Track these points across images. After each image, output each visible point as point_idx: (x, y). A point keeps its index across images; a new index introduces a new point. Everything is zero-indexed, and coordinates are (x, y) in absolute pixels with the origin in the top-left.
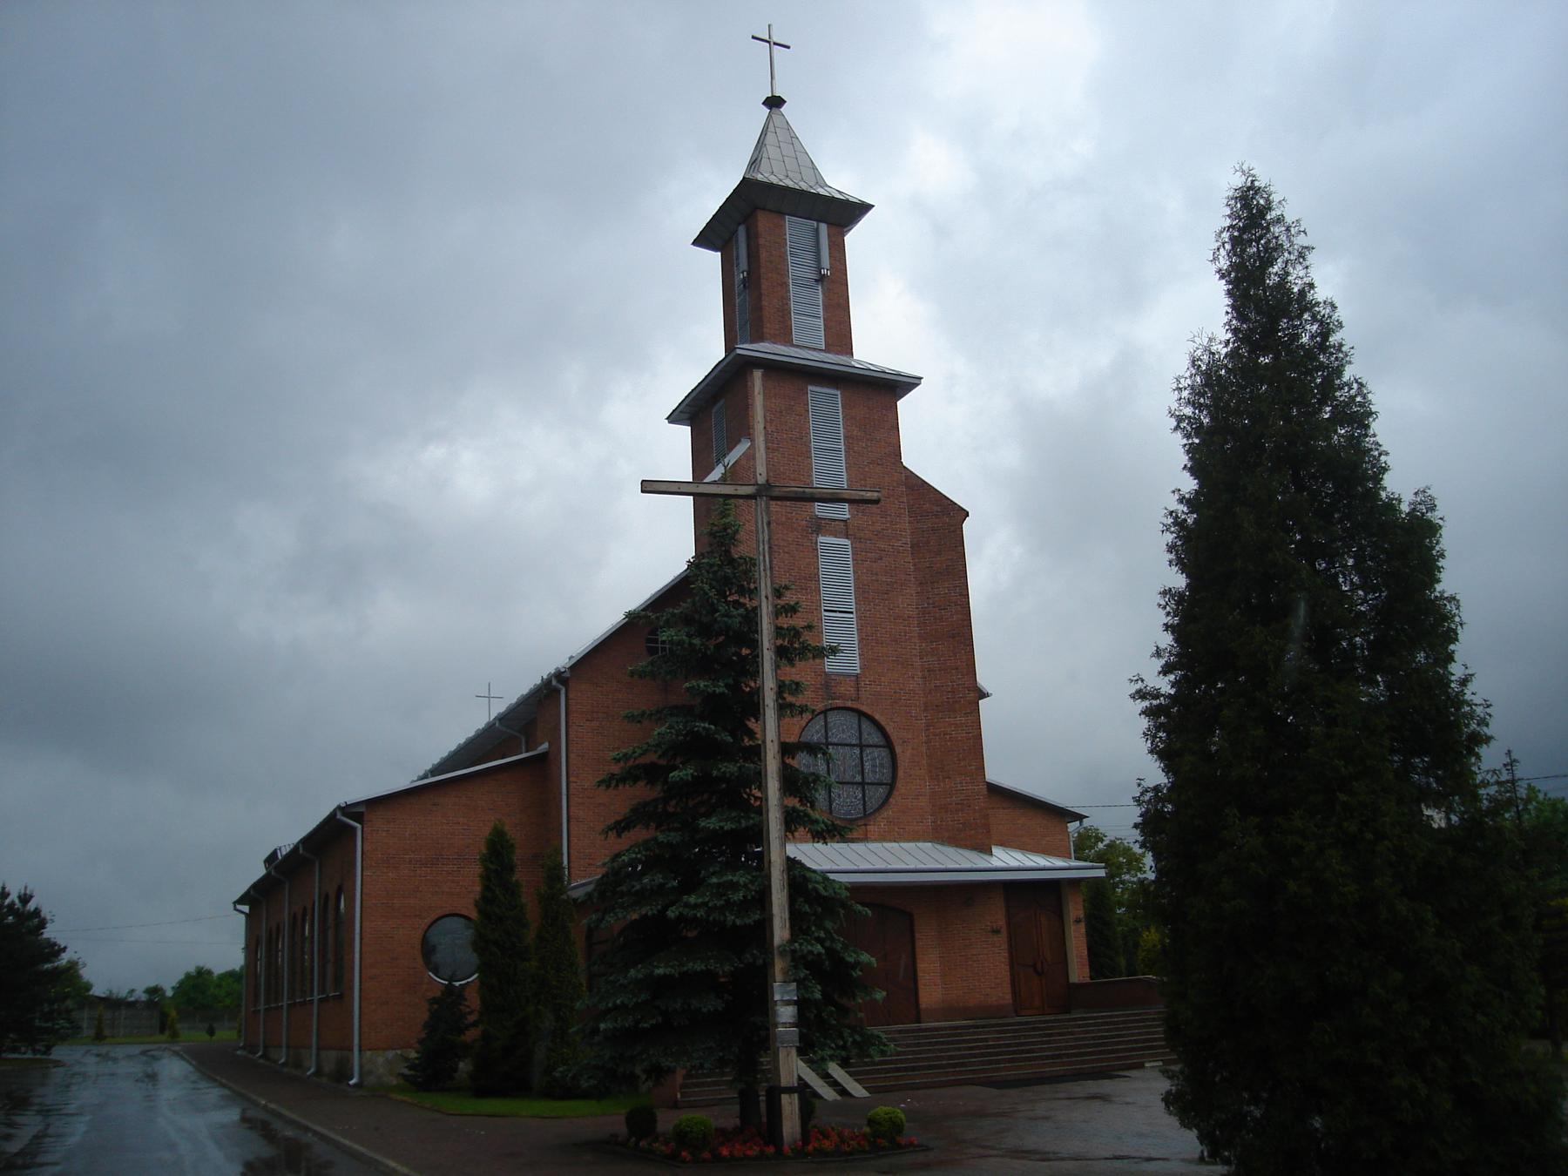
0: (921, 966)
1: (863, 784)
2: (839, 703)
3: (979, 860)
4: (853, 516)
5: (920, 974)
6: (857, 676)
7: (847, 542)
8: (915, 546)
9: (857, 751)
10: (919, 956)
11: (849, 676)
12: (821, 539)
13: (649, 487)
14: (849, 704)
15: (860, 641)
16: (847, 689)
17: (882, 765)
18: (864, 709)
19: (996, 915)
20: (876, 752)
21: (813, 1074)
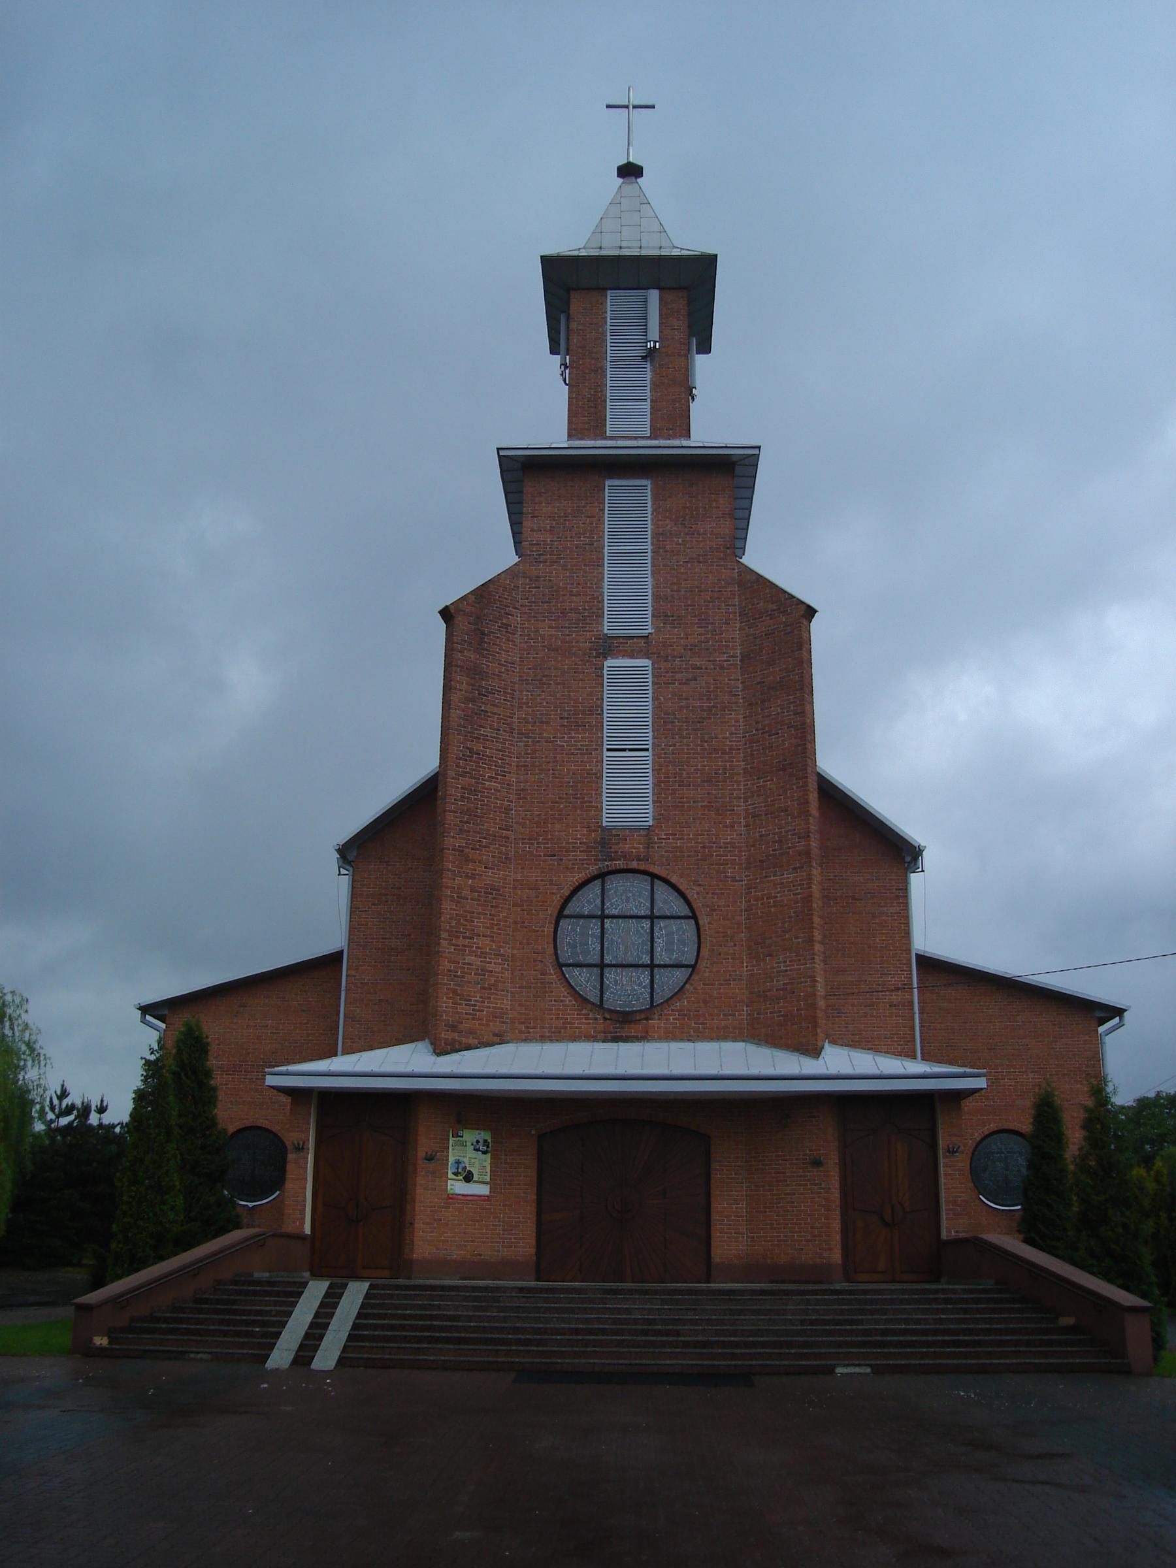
0: (717, 1205)
1: (652, 966)
2: (619, 864)
3: (809, 1066)
4: (658, 630)
5: (715, 1217)
6: (648, 829)
7: (646, 662)
8: (745, 657)
9: (646, 924)
10: (715, 1192)
11: (638, 829)
12: (609, 662)
13: (608, 106)
14: (634, 865)
15: (657, 784)
16: (635, 846)
17: (682, 942)
18: (656, 870)
19: (824, 1140)
20: (674, 925)
21: (209, 1244)
